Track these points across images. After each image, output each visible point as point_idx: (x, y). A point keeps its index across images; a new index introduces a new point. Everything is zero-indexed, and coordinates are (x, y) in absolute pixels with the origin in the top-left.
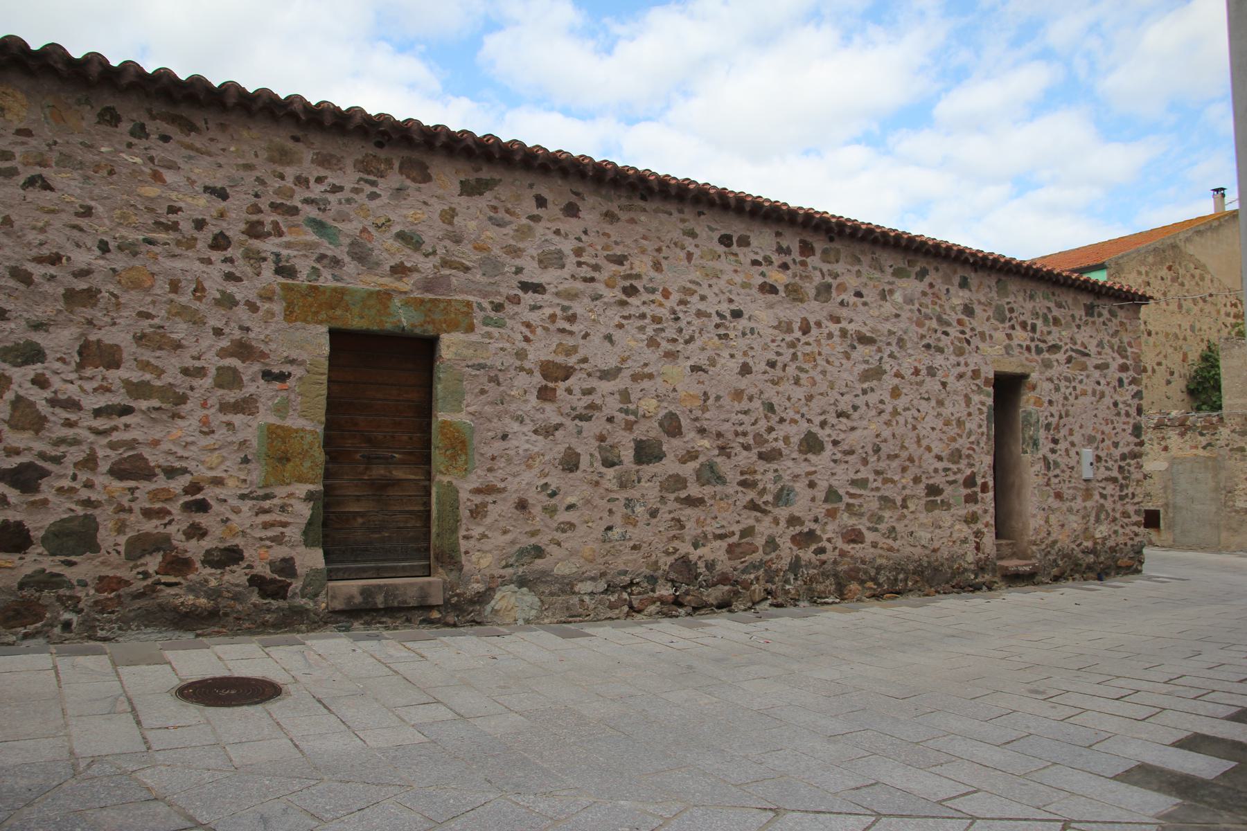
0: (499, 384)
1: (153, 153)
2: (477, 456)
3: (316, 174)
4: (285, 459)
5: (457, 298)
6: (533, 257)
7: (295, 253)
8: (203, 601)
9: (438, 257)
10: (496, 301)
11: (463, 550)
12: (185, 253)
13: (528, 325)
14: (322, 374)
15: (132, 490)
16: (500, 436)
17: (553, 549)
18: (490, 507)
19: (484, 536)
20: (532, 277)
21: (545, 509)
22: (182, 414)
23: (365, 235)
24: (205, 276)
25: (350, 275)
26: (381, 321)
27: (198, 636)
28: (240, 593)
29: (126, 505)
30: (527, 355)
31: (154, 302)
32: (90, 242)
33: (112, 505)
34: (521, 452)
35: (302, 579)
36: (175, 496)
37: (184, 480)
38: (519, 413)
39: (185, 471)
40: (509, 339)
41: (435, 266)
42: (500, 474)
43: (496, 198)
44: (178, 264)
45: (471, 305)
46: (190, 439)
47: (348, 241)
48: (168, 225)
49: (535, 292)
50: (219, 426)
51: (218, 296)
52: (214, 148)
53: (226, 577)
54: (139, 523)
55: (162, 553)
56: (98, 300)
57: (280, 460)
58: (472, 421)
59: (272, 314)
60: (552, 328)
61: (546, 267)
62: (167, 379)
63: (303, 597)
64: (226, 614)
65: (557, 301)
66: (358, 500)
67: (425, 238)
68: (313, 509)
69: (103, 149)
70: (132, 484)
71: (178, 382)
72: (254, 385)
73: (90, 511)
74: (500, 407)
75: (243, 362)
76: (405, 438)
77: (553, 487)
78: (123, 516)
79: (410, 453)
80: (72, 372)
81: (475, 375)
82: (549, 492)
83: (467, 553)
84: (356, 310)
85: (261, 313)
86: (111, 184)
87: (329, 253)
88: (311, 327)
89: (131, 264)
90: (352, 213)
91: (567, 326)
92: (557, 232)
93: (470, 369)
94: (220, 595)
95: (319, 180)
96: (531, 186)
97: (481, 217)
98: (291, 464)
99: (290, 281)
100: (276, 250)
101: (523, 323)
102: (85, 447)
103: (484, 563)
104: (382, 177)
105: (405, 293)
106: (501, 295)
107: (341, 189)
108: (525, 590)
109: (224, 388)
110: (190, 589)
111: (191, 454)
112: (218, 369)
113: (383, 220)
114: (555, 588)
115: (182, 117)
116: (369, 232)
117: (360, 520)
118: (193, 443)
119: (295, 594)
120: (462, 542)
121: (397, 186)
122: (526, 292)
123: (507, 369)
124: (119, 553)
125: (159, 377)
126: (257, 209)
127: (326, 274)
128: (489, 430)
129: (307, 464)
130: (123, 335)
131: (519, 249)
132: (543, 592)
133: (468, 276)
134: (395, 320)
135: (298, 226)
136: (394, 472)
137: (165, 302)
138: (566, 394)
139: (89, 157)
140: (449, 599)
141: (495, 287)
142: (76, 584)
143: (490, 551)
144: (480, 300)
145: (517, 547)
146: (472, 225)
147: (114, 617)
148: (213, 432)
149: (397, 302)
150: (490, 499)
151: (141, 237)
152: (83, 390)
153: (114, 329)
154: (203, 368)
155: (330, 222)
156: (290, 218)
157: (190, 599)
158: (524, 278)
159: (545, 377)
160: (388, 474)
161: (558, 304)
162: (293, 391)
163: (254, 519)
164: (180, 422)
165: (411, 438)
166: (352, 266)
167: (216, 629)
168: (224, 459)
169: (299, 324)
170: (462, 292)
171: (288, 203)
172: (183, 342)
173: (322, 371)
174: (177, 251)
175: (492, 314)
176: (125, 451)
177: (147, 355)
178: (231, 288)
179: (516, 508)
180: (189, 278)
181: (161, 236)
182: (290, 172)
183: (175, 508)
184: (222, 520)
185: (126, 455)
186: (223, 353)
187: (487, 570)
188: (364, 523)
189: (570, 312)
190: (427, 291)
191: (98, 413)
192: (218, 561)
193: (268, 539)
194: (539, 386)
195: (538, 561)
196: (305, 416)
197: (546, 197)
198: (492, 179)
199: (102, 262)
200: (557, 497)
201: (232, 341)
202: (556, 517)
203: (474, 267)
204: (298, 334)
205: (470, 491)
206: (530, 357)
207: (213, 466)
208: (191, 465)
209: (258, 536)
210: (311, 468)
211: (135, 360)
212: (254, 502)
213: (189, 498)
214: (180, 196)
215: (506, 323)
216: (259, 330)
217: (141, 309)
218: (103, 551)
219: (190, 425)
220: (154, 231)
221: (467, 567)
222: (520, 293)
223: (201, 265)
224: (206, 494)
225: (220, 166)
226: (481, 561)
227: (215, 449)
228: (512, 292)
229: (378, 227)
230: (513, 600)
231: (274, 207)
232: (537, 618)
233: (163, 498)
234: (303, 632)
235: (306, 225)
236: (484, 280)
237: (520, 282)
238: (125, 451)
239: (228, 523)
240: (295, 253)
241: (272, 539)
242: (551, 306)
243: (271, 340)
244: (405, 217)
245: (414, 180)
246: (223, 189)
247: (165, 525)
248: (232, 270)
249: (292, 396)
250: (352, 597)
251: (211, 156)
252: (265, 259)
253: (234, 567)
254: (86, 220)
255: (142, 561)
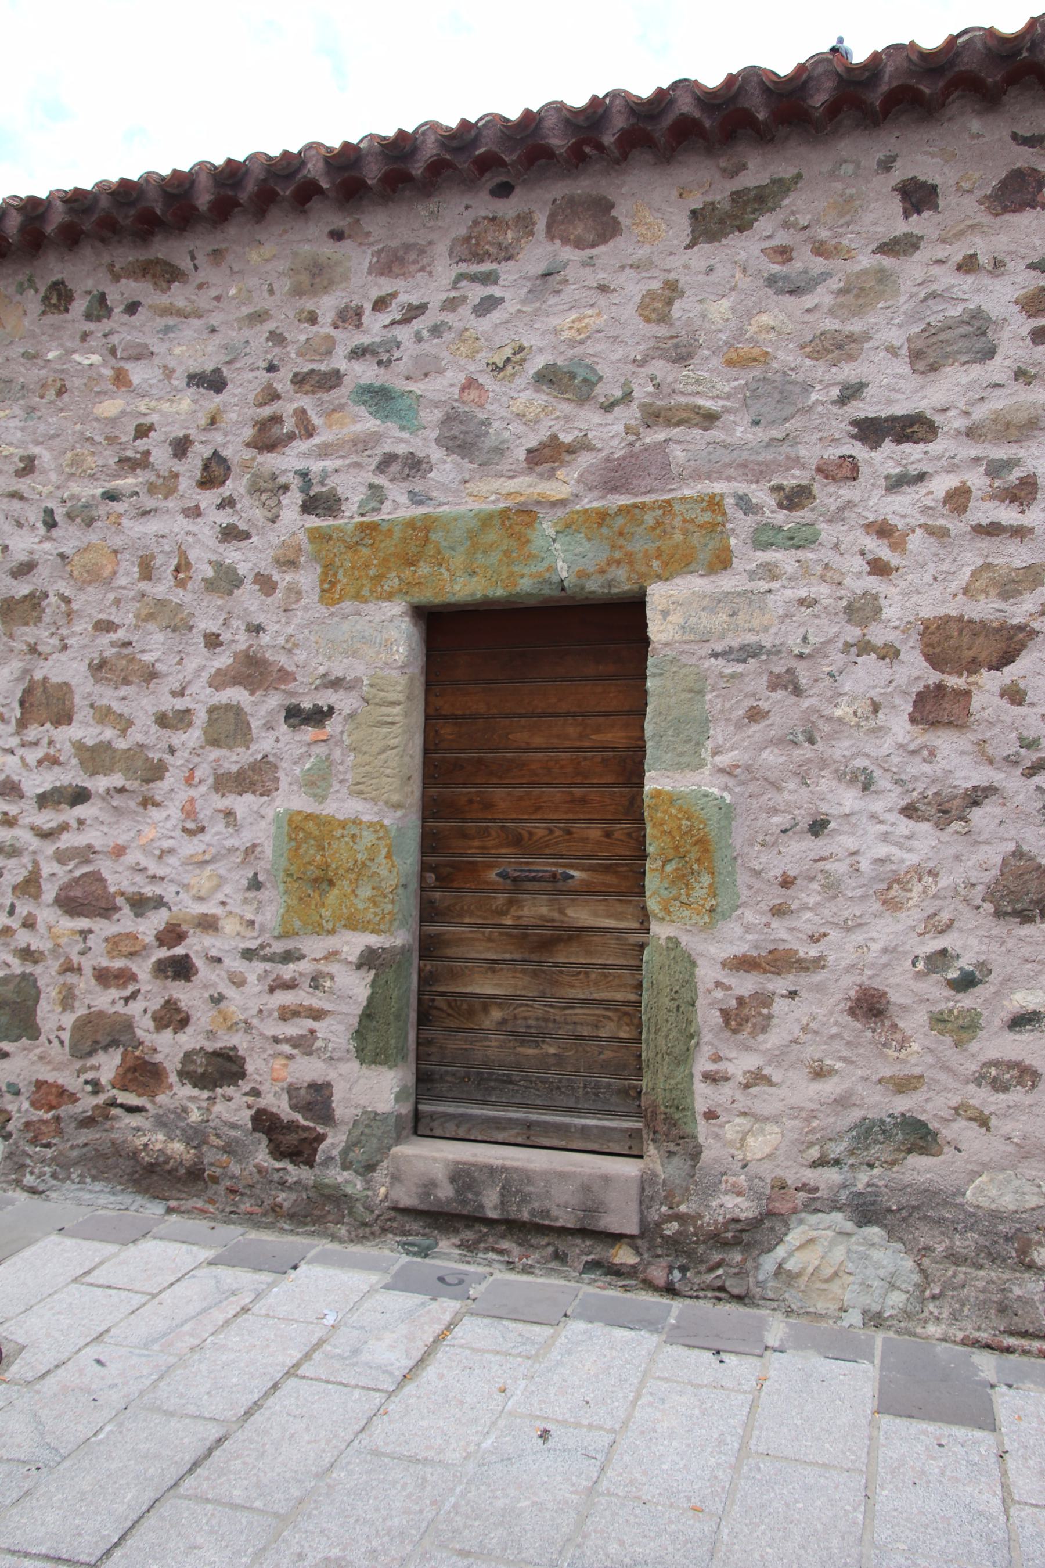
0: (797, 691)
1: (115, 339)
2: (743, 878)
3: (375, 294)
4: (324, 881)
5: (687, 492)
6: (892, 351)
7: (339, 463)
8: (177, 1147)
9: (634, 405)
10: (790, 482)
11: (700, 1106)
12: (164, 504)
13: (883, 530)
14: (393, 704)
15: (84, 934)
16: (804, 825)
17: (961, 1131)
18: (780, 1006)
19: (757, 1078)
20: (890, 402)
21: (939, 1021)
22: (158, 798)
23: (473, 394)
24: (190, 539)
25: (443, 487)
26: (511, 574)
27: (170, 1211)
28: (237, 1141)
29: (75, 959)
30: (879, 610)
31: (117, 602)
32: (34, 515)
33: (57, 958)
34: (865, 865)
35: (346, 1129)
36: (145, 947)
37: (155, 921)
38: (860, 763)
39: (159, 902)
40: (828, 574)
41: (628, 430)
42: (807, 922)
43: (786, 225)
44: (152, 526)
45: (719, 504)
46: (166, 844)
47: (438, 415)
48: (136, 459)
49: (899, 440)
50: (211, 818)
51: (210, 573)
52: (203, 301)
53: (219, 1108)
54: (90, 992)
55: (121, 1049)
56: (43, 611)
57: (316, 882)
58: (726, 788)
59: (295, 592)
60: (956, 526)
61: (933, 368)
62: (136, 736)
63: (345, 1167)
64: (215, 1180)
65: (976, 450)
66: (494, 971)
67: (602, 369)
68: (373, 984)
69: (50, 356)
70: (83, 923)
71: (150, 741)
72: (272, 735)
73: (29, 969)
74: (806, 751)
75: (252, 694)
76: (595, 833)
77: (966, 962)
78: (71, 978)
79: (607, 869)
80: (12, 735)
81: (733, 676)
82: (953, 974)
83: (710, 1115)
84: (458, 560)
85: (279, 594)
86: (61, 410)
87: (401, 449)
88: (371, 608)
89: (86, 540)
90: (445, 354)
91: (1007, 515)
92: (969, 265)
93: (721, 662)
94: (205, 1142)
95: (381, 304)
96: (886, 165)
97: (744, 282)
98: (336, 891)
99: (331, 522)
100: (301, 465)
101: (868, 527)
102: (26, 859)
103: (758, 1146)
104: (508, 258)
105: (563, 503)
106: (803, 467)
107: (420, 309)
108: (874, 1232)
109: (219, 746)
110: (161, 1123)
111: (168, 870)
112: (211, 711)
113: (508, 352)
114: (966, 1243)
115: (158, 262)
116: (481, 386)
117: (496, 1014)
118: (171, 851)
119: (331, 1158)
120: (700, 1088)
121: (542, 268)
122: (875, 445)
123: (820, 652)
124: (62, 1043)
125: (124, 732)
126: (272, 396)
127: (397, 493)
128: (775, 811)
129: (365, 892)
130: (75, 665)
131: (851, 337)
132: (927, 1248)
133: (716, 434)
134: (541, 567)
135: (341, 407)
136: (571, 912)
137: (133, 599)
138: (1004, 703)
139: (34, 374)
140: (658, 1225)
141: (785, 449)
142: (4, 1089)
143: (775, 1119)
144: (742, 488)
145: (855, 1115)
146: (721, 309)
147: (49, 1153)
148: (202, 830)
149: (548, 527)
150: (779, 985)
151: (100, 491)
152: (25, 764)
153: (64, 657)
154: (188, 711)
155: (402, 385)
156: (326, 396)
157: (158, 1139)
158: (866, 409)
159: (936, 661)
160: (556, 915)
161: (977, 460)
162: (339, 743)
163: (265, 998)
164: (155, 813)
165: (608, 834)
166: (448, 467)
167: (200, 1204)
168: (222, 881)
169: (347, 605)
170: (698, 475)
171: (323, 367)
172: (159, 666)
173: (392, 697)
174: (149, 503)
175: (780, 517)
176: (76, 867)
177: (108, 696)
178: (233, 555)
179: (852, 1012)
180: (167, 548)
181: (127, 483)
182: (327, 305)
183: (143, 969)
184: (211, 997)
185: (77, 873)
186: (220, 680)
187: (767, 1165)
188: (504, 1021)
189: (1016, 475)
190: (614, 490)
191: (44, 800)
192: (203, 1074)
193: (288, 1040)
194: (919, 687)
195: (915, 1160)
196: (360, 793)
197: (937, 180)
198: (778, 182)
199: (47, 546)
200: (979, 990)
201: (236, 655)
202: (974, 1047)
203: (727, 410)
204: (346, 626)
205: (724, 964)
206: (888, 613)
207: (202, 893)
208: (167, 891)
209: (270, 1033)
210: (373, 900)
211: (92, 706)
212: (268, 966)
213: (164, 953)
214: (153, 403)
215: (818, 533)
216: (277, 627)
217: (101, 616)
218: (43, 1038)
219: (168, 817)
220: (117, 476)
221: (711, 1152)
222: (859, 451)
223: (185, 521)
224: (190, 947)
225: (213, 331)
226: (750, 1140)
227: (207, 862)
228: (833, 453)
229: (497, 369)
230: (839, 1253)
231: (299, 380)
232: (908, 1315)
233: (126, 949)
234: (341, 1241)
235: (355, 402)
236: (760, 434)
237: (855, 423)
238: (76, 867)
239: (223, 1005)
240: (339, 463)
241: (296, 1042)
242: (952, 468)
243: (296, 645)
244: (556, 332)
245: (579, 244)
246: (217, 371)
247: (127, 1000)
248: (234, 520)
249: (337, 754)
250: (430, 1185)
251: (200, 317)
252: (286, 488)
253: (230, 1091)
254: (28, 480)
255: (93, 1061)
